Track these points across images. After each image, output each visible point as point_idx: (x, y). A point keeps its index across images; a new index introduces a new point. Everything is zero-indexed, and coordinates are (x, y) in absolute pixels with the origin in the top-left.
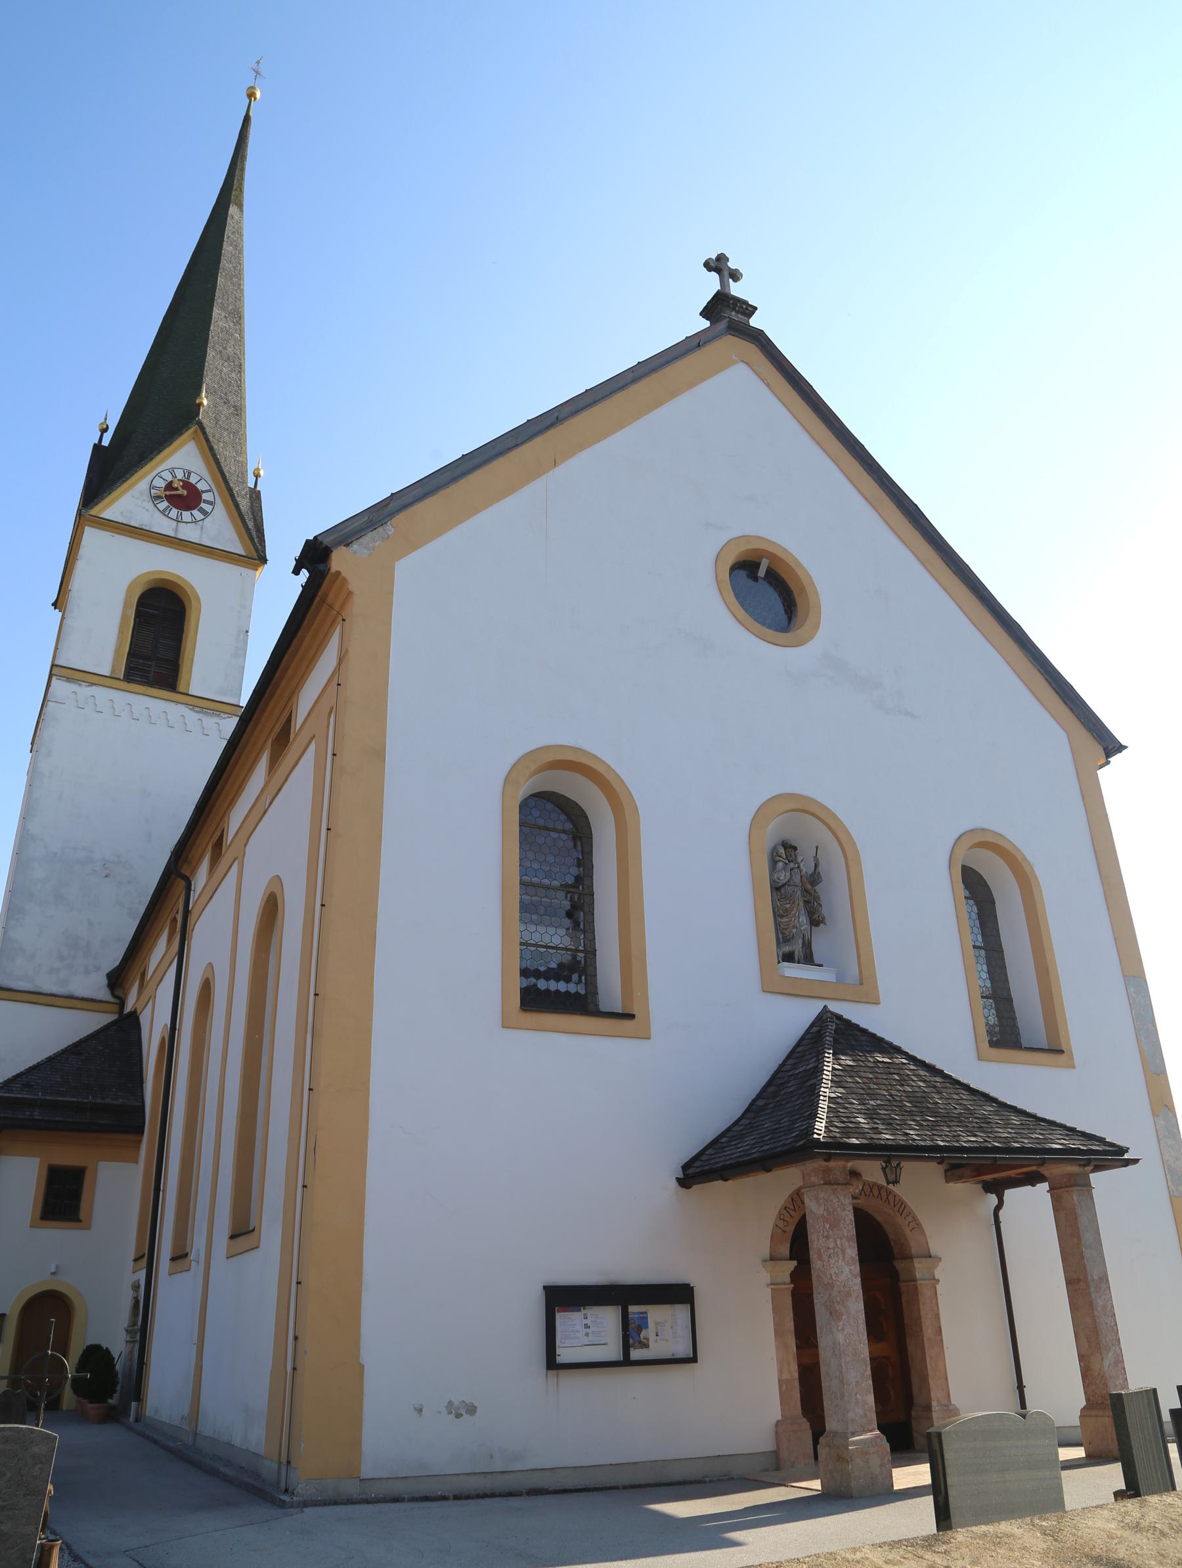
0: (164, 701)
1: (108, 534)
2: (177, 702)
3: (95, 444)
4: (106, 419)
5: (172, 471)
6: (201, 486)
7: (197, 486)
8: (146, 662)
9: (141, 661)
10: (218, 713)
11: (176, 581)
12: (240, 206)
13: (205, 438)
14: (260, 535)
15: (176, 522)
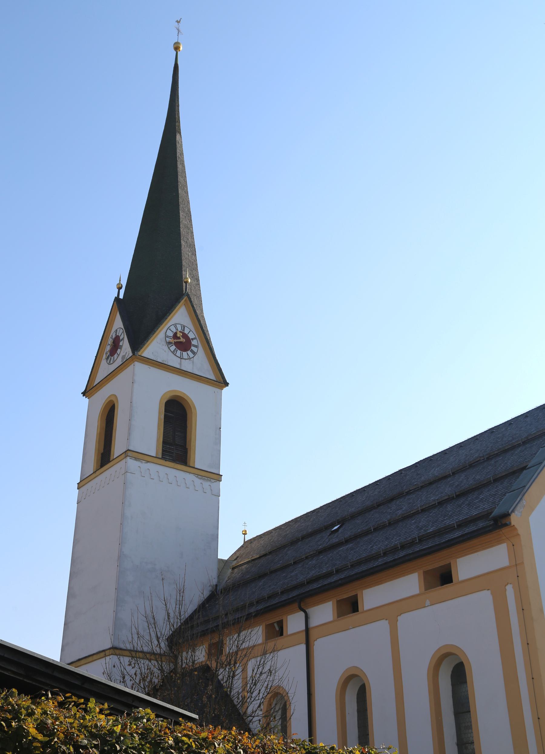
0: (183, 472)
1: (147, 366)
2: (190, 473)
3: (116, 297)
4: (120, 280)
5: (175, 325)
6: (191, 336)
7: (189, 335)
8: (171, 447)
9: (168, 446)
10: (210, 479)
11: (183, 396)
12: (180, 133)
13: (192, 306)
14: (219, 369)
15: (180, 359)
